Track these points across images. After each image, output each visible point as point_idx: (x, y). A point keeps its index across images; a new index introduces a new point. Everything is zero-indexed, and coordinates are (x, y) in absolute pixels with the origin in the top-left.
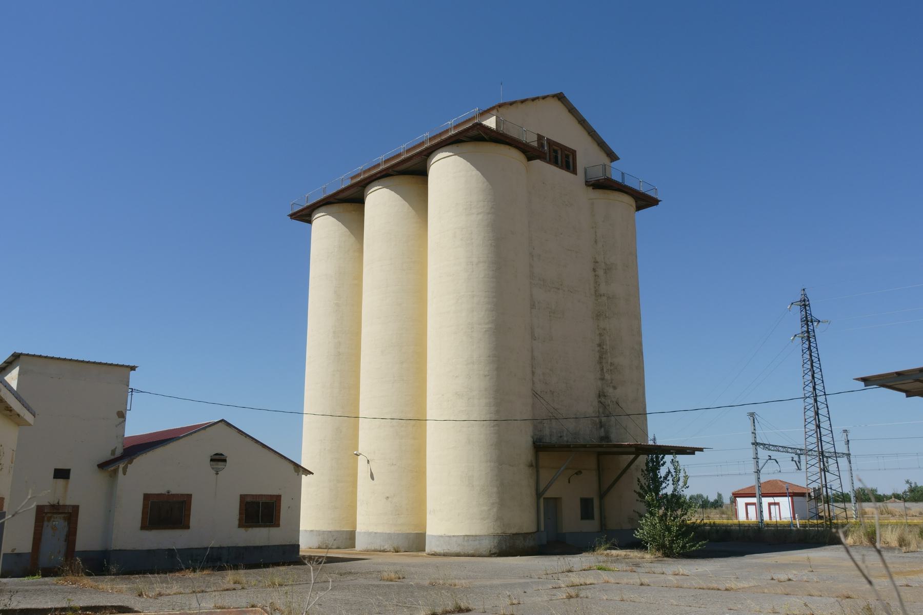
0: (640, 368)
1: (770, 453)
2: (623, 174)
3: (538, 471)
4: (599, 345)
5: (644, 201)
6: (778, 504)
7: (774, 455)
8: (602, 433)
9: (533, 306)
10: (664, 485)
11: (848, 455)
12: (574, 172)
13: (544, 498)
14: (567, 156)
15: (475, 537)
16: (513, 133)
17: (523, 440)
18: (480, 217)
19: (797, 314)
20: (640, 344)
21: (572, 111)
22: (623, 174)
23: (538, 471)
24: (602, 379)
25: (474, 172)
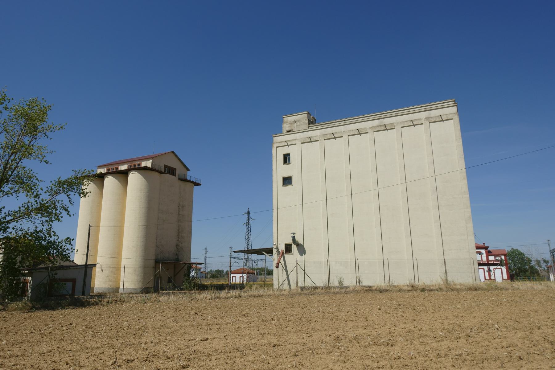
0: (190, 237)
1: (236, 260)
2: (190, 176)
3: (155, 269)
4: (178, 230)
5: (196, 184)
6: (235, 277)
7: (237, 260)
8: (176, 257)
9: (158, 219)
10: (191, 274)
11: (266, 260)
12: (175, 176)
13: (157, 277)
14: (173, 170)
15: (135, 289)
16: (156, 168)
17: (152, 262)
18: (145, 193)
19: (246, 216)
20: (191, 230)
21: (176, 156)
22: (190, 176)
23: (155, 269)
24: (178, 241)
25: (144, 179)
